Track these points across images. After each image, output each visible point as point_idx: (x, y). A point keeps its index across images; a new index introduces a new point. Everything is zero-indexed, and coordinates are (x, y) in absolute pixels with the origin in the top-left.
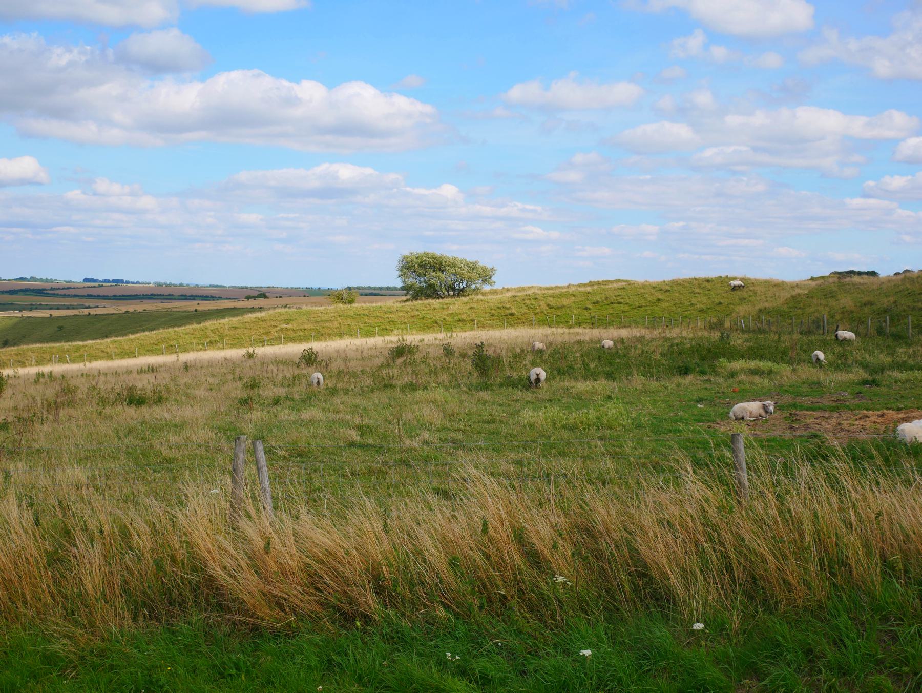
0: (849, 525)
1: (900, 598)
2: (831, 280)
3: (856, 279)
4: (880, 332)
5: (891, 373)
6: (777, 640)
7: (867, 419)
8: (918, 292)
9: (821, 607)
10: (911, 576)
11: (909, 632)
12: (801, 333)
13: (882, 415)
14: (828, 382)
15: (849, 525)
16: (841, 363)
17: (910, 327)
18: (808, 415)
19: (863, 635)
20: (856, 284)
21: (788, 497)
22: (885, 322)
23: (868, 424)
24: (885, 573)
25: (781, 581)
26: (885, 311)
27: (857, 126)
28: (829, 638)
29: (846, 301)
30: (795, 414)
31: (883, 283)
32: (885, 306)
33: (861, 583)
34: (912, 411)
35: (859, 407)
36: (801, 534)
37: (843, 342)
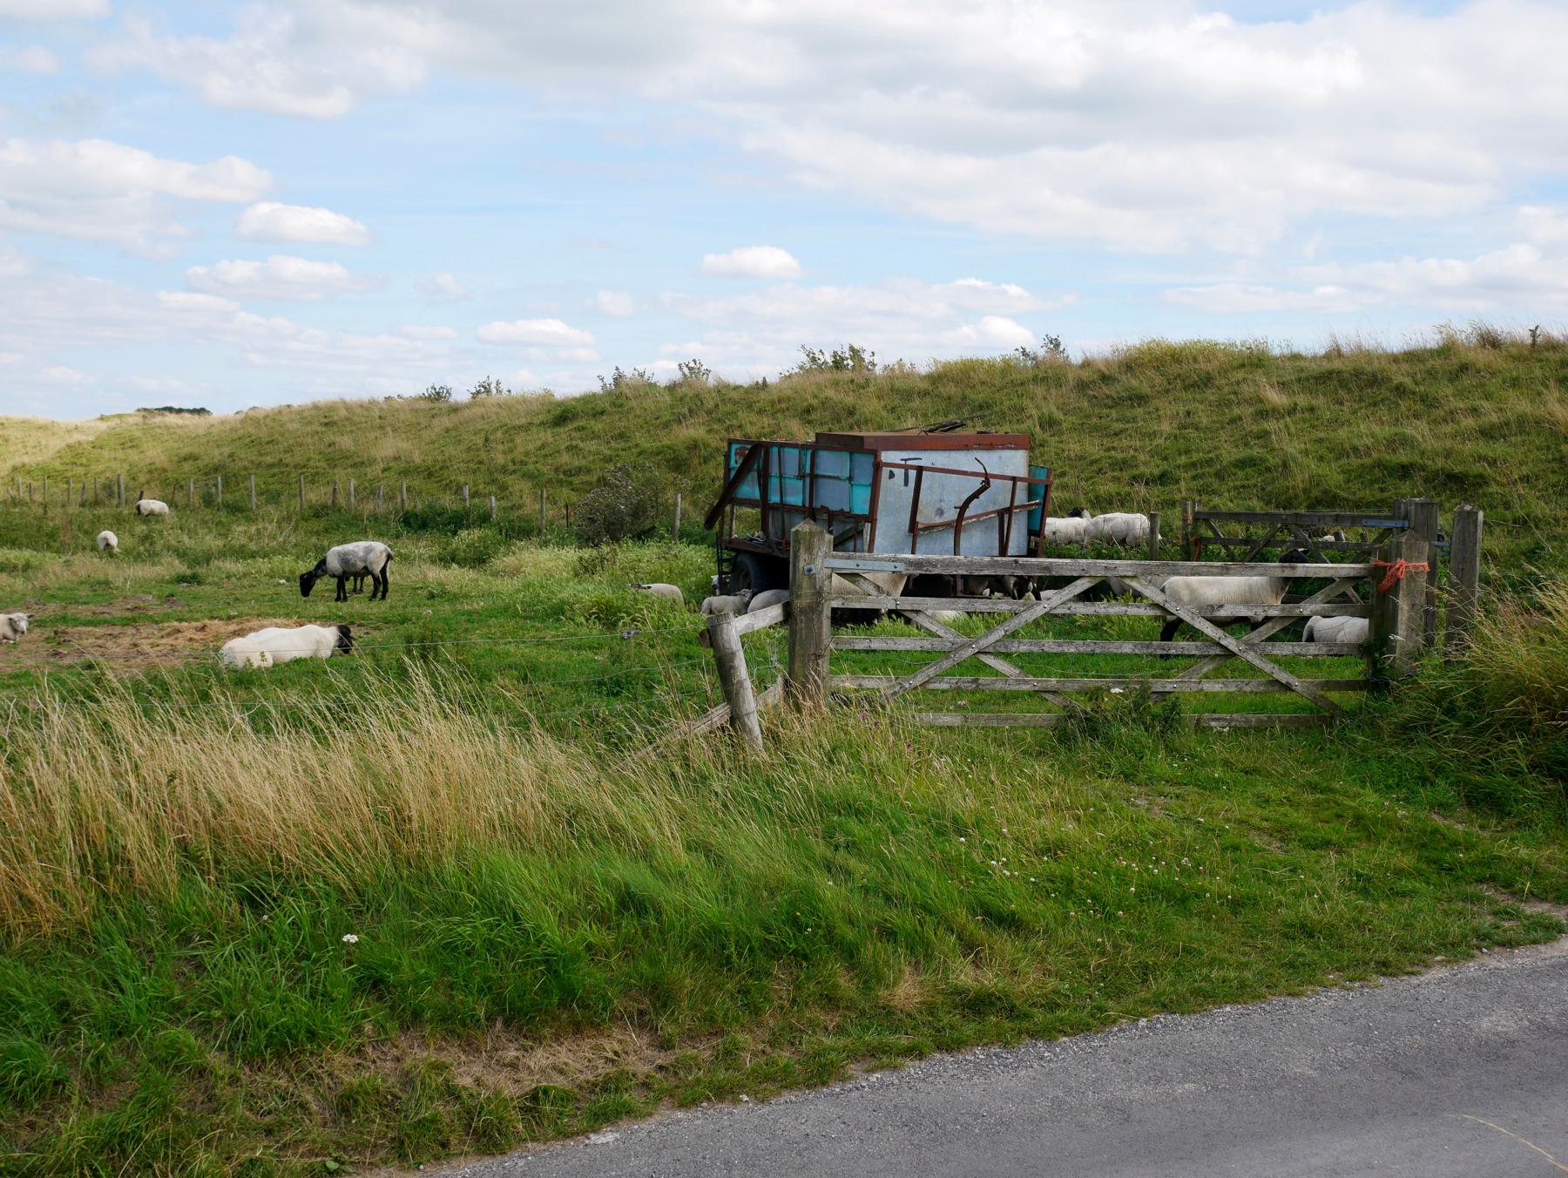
0: (127, 798)
1: (208, 903)
2: (131, 420)
3: (171, 419)
4: (208, 501)
5: (221, 564)
6: (9, 995)
7: (179, 635)
8: (267, 440)
9: (83, 933)
10: (224, 868)
11: (223, 955)
12: (82, 505)
13: (203, 628)
14: (121, 580)
15: (127, 798)
16: (144, 552)
17: (254, 492)
18: (84, 633)
19: (150, 969)
20: (173, 427)
21: (28, 761)
22: (216, 485)
23: (180, 642)
24: (186, 868)
25: (16, 898)
26: (216, 469)
27: (178, 176)
28: (96, 980)
29: (155, 454)
30: (64, 633)
31: (213, 425)
32: (216, 461)
33: (147, 887)
34: (248, 621)
35: (167, 617)
36: (49, 815)
37: (150, 517)
